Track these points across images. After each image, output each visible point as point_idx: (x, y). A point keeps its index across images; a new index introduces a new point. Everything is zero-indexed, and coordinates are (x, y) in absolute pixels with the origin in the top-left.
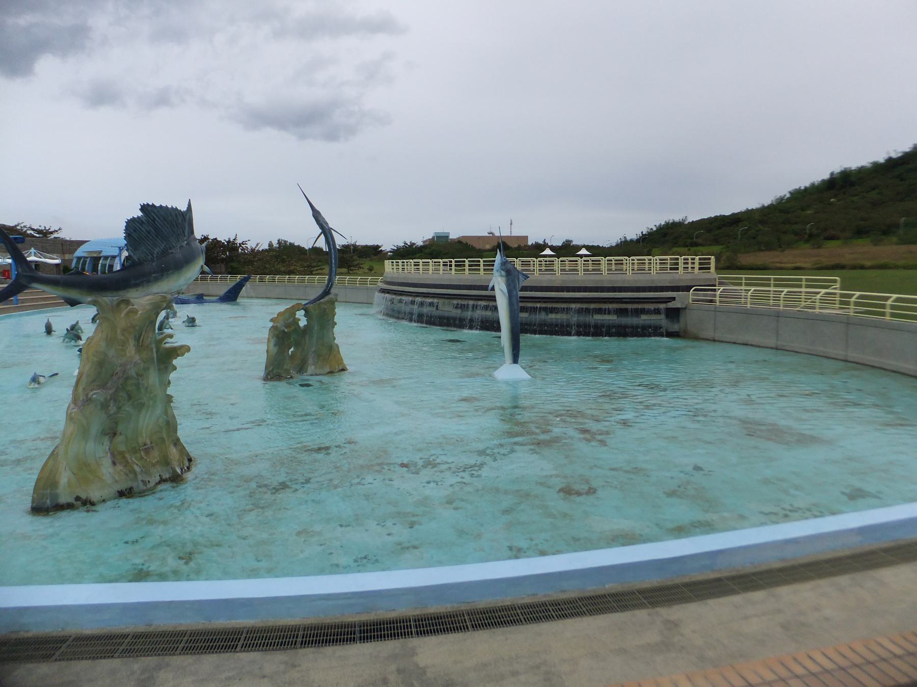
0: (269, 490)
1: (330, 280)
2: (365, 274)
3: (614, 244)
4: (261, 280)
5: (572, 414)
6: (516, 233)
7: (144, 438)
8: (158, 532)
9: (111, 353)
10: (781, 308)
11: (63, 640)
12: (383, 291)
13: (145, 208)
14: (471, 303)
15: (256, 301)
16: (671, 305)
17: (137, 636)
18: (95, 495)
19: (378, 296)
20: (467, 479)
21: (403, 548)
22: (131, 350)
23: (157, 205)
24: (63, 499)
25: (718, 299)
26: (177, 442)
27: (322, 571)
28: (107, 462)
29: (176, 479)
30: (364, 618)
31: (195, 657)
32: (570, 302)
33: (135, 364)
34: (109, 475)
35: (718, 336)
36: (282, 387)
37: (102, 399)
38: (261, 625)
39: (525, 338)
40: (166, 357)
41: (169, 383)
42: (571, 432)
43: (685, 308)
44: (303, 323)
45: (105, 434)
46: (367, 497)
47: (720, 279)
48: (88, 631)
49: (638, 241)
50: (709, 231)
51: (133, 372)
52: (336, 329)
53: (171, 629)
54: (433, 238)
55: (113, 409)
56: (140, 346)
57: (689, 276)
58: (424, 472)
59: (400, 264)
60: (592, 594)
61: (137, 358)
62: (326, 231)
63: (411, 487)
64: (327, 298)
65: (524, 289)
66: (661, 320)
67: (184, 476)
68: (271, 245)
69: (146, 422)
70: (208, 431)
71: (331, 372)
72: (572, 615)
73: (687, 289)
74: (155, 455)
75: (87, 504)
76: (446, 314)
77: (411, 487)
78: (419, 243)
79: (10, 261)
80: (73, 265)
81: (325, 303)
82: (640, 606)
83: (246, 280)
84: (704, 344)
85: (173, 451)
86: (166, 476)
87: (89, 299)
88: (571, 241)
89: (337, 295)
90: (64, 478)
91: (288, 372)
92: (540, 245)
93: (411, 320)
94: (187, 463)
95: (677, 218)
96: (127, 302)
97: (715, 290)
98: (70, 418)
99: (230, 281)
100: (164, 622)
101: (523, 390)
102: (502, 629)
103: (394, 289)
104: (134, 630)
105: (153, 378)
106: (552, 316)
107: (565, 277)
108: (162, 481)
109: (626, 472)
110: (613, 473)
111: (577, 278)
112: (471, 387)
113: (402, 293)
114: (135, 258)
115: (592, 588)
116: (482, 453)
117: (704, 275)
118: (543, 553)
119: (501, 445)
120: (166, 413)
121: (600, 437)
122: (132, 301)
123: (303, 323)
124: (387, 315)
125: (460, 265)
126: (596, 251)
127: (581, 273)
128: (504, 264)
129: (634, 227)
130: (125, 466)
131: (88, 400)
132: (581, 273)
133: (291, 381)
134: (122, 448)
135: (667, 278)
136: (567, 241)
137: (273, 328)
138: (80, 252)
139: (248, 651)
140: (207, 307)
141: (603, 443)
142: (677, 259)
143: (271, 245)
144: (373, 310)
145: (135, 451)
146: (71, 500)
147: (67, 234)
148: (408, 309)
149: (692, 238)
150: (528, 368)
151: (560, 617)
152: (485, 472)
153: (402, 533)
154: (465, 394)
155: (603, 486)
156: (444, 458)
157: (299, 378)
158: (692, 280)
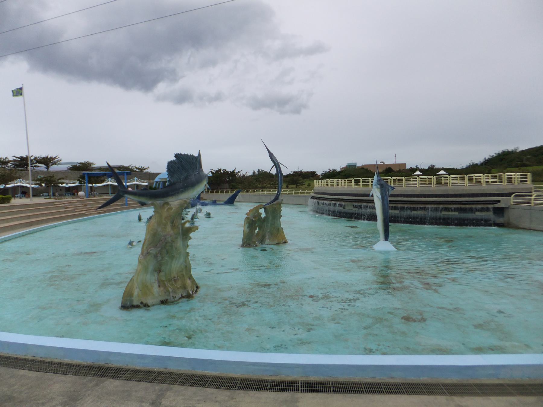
0: (234, 306)
1: (278, 191)
2: (306, 188)
3: (464, 167)
4: (247, 192)
5: (420, 272)
6: (399, 162)
7: (174, 274)
8: (175, 322)
9: (159, 229)
11: (126, 370)
12: (313, 198)
13: (177, 156)
14: (364, 204)
15: (244, 204)
16: (497, 206)
17: (160, 373)
18: (150, 301)
19: (310, 201)
20: (346, 307)
21: (302, 343)
22: (169, 228)
23: (183, 154)
24: (135, 303)
25: (533, 201)
26: (191, 277)
27: (255, 351)
28: (156, 285)
29: (189, 297)
30: (274, 378)
31: (185, 387)
32: (427, 204)
33: (171, 235)
34: (157, 292)
35: (533, 226)
36: (251, 251)
37: (154, 253)
38: (219, 375)
39: (393, 227)
40: (186, 233)
41: (188, 246)
42: (417, 283)
43: (508, 208)
44: (263, 215)
45: (156, 271)
46: (286, 312)
47: (536, 188)
48: (138, 368)
49: (482, 164)
50: (536, 156)
51: (169, 240)
52: (282, 219)
53: (176, 372)
54: (347, 167)
55: (159, 258)
56: (173, 226)
57: (511, 187)
58: (321, 301)
59: (320, 182)
60: (410, 382)
61: (172, 232)
62: (276, 164)
63: (310, 308)
64: (277, 202)
65: (392, 196)
66: (490, 215)
67: (194, 295)
68: (254, 172)
69: (176, 266)
70: (208, 273)
71: (278, 244)
72: (396, 393)
73: (509, 195)
74: (179, 284)
75: (146, 306)
76: (349, 211)
77: (310, 308)
78: (338, 170)
79: (116, 184)
80: (154, 186)
81: (275, 205)
82: (442, 394)
83: (238, 192)
84: (521, 231)
85: (188, 282)
86: (184, 295)
87: (150, 202)
88: (434, 166)
89: (282, 200)
90: (136, 292)
91: (254, 242)
92: (413, 169)
93: (329, 215)
94: (195, 289)
95: (510, 148)
96: (167, 204)
97: (531, 196)
98: (140, 262)
99: (229, 194)
100: (173, 368)
101: (392, 257)
102: (355, 395)
103: (319, 197)
104: (159, 370)
105: (179, 243)
106: (415, 212)
107: (423, 188)
108: (182, 297)
109: (449, 310)
110: (440, 310)
111: (431, 189)
112: (359, 254)
113: (324, 199)
114: (172, 181)
115: (411, 378)
116: (358, 292)
117: (523, 186)
118: (384, 354)
119: (370, 289)
120: (185, 262)
121: (434, 288)
122: (170, 203)
123: (263, 215)
124: (314, 211)
125: (357, 182)
126: (450, 171)
127: (418, 186)
128: (379, 181)
129: (479, 156)
130: (165, 288)
131: (148, 253)
132: (433, 186)
133: (256, 248)
134: (163, 279)
135: (494, 188)
136: (431, 166)
137: (247, 218)
138: (157, 179)
139: (211, 388)
140: (218, 208)
141: (436, 291)
143: (254, 172)
144: (307, 209)
145: (169, 280)
146: (139, 304)
147: (152, 170)
148: (327, 208)
149: (522, 161)
150: (396, 244)
151: (388, 393)
152: (358, 304)
153: (303, 335)
154: (354, 258)
155: (432, 317)
156: (335, 294)
157: (260, 246)
158: (512, 189)
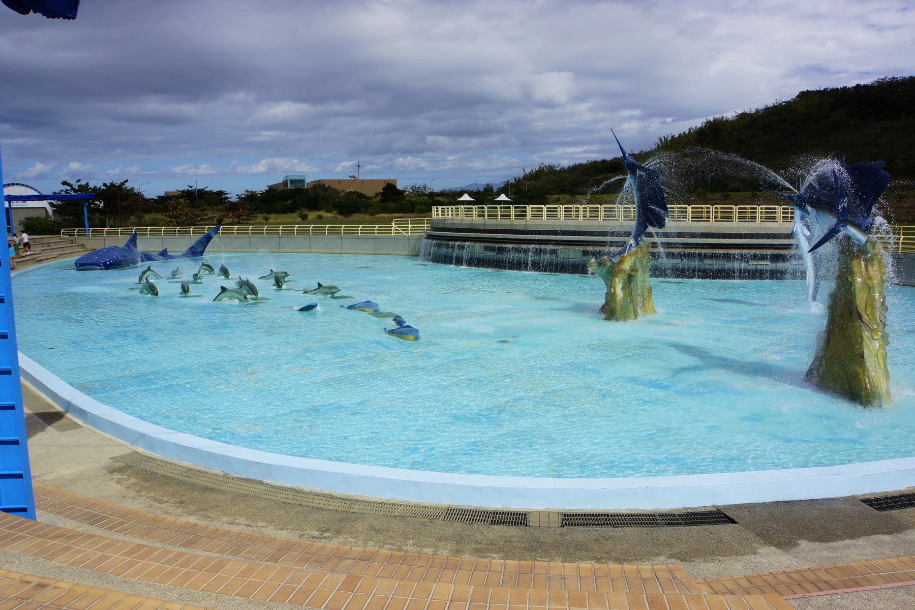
35: (378, 252)
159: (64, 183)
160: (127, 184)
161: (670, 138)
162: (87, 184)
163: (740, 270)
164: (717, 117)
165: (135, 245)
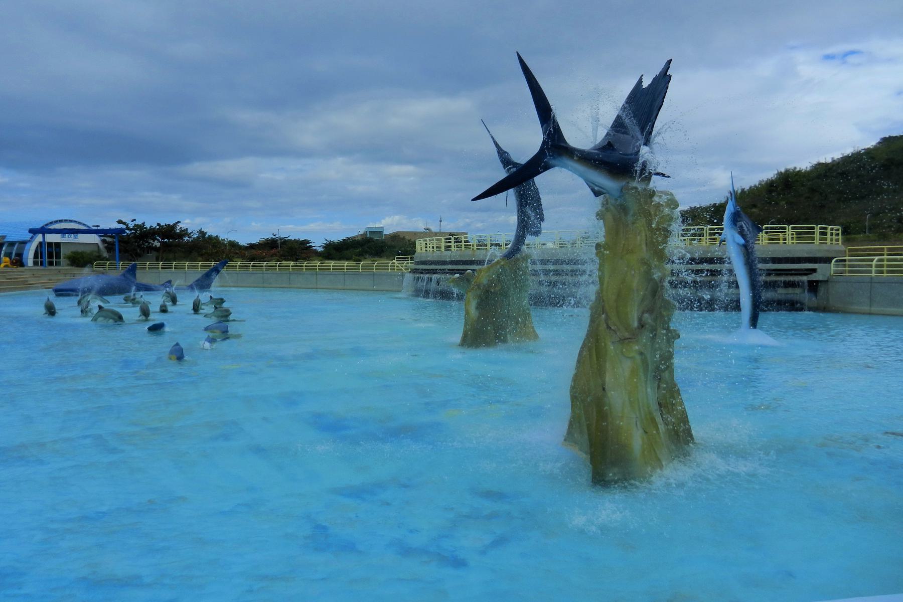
10: (873, 274)
35: (874, 309)
73: (828, 260)
84: (853, 317)
113: (434, 272)
142: (826, 229)
158: (828, 251)
159: (120, 222)
160: (180, 225)
161: (739, 191)
162: (144, 223)
163: (692, 309)
164: (789, 167)
165: (134, 275)
